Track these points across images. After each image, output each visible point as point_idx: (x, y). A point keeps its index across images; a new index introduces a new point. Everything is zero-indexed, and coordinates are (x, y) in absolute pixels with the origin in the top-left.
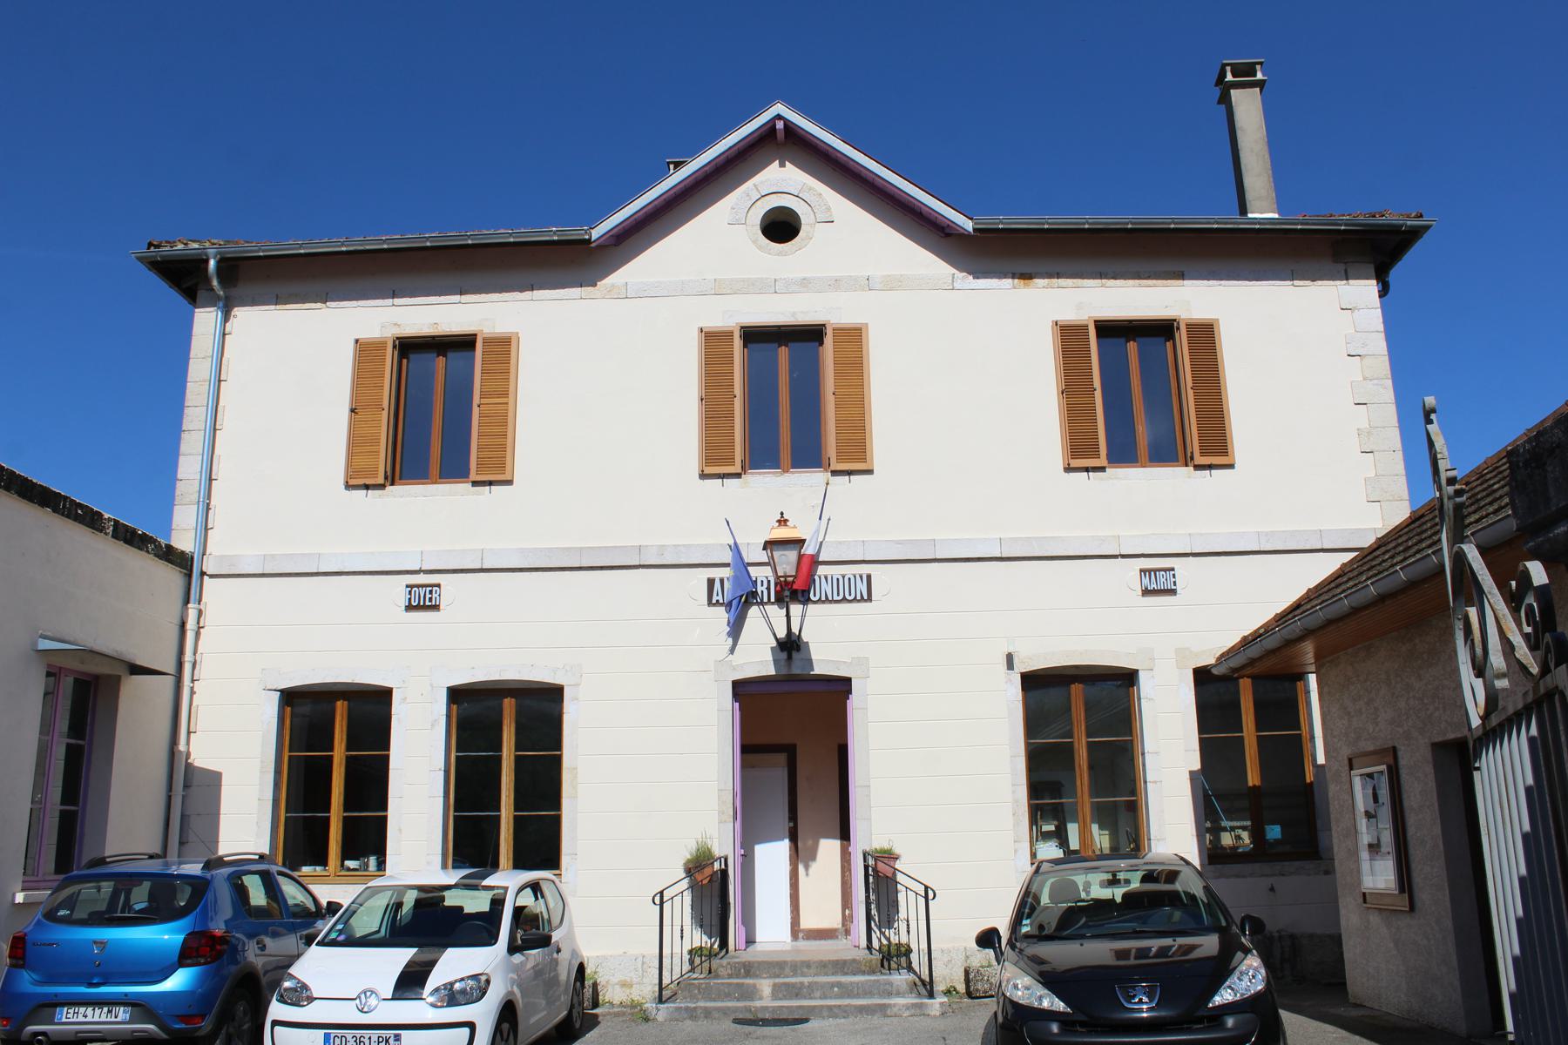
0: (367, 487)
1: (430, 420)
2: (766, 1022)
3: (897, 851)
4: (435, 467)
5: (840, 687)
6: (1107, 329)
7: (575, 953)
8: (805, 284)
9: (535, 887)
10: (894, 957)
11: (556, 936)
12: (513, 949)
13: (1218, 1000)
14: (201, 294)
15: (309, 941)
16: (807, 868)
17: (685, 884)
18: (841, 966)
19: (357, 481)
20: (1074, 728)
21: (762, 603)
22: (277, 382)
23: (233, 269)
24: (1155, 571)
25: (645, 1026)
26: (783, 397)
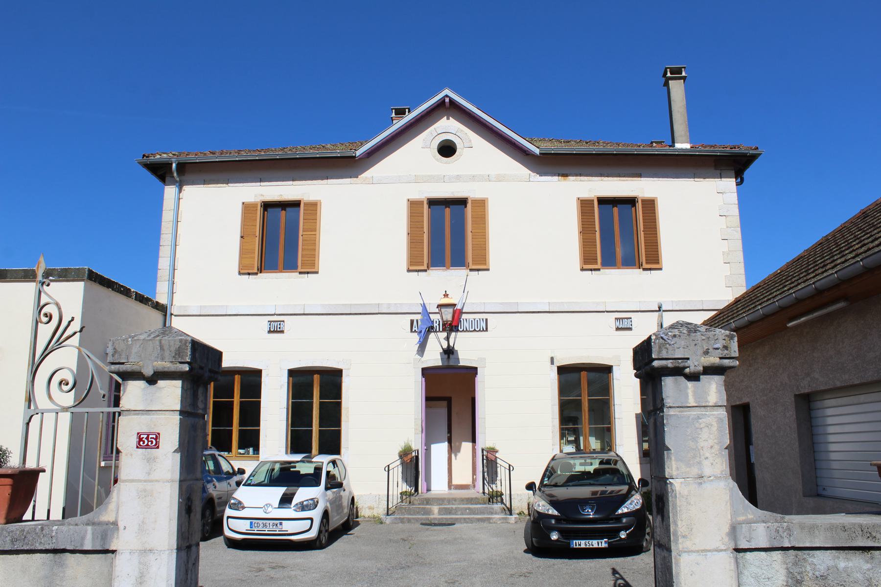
0: (249, 274)
1: (279, 242)
2: (435, 525)
3: (497, 448)
4: (281, 265)
5: (474, 371)
6: (603, 201)
7: (350, 493)
8: (458, 178)
9: (334, 462)
10: (495, 497)
11: (345, 483)
12: (327, 489)
13: (620, 511)
14: (168, 179)
15: (238, 484)
16: (456, 456)
17: (399, 462)
18: (470, 501)
19: (245, 271)
20: (582, 393)
21: (436, 331)
22: (206, 221)
23: (183, 167)
24: (622, 319)
25: (381, 526)
26: (447, 232)
